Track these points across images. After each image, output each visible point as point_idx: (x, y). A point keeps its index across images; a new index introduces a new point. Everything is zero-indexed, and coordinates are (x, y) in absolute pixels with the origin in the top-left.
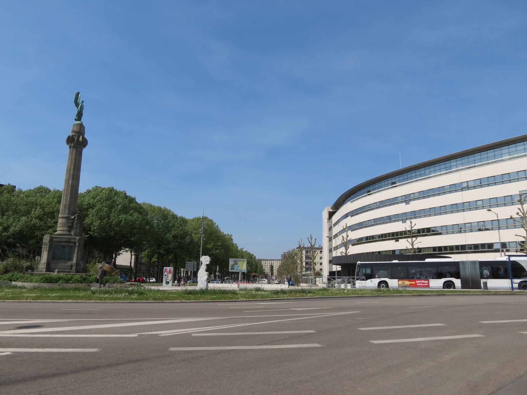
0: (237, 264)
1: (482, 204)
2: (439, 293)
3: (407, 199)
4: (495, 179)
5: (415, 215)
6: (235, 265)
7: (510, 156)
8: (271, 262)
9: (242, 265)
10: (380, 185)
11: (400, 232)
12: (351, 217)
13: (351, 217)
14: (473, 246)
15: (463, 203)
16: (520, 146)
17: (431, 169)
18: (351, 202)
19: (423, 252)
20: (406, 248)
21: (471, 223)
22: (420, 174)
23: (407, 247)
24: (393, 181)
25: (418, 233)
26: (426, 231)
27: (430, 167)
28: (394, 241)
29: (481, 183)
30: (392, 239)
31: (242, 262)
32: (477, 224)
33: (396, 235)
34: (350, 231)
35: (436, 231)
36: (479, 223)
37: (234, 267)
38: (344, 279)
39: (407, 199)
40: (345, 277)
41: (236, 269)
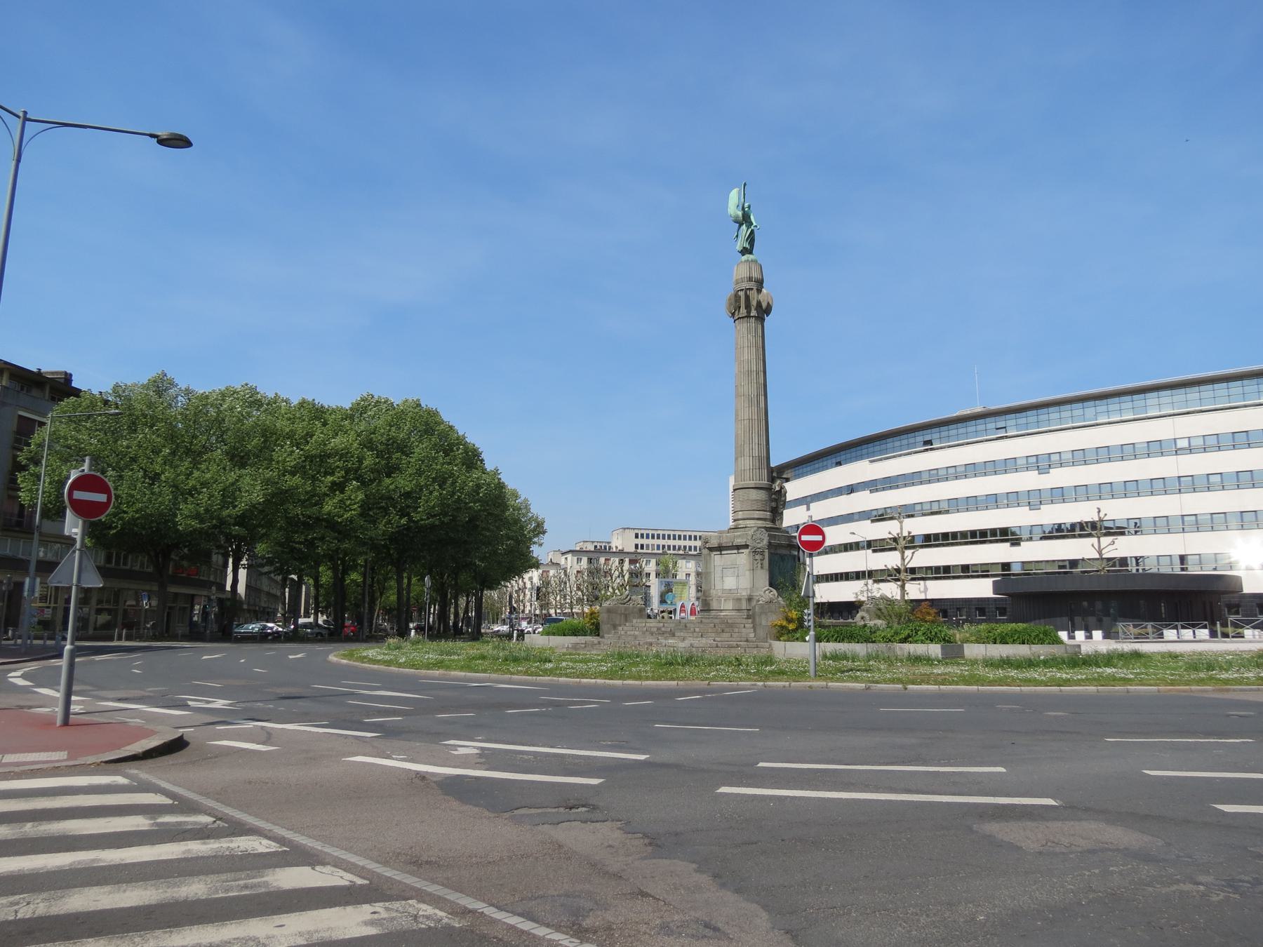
0: (672, 592)
1: (1220, 480)
2: (133, 609)
3: (1042, 464)
4: (1247, 436)
5: (909, 512)
6: (668, 593)
7: (1134, 415)
8: (1138, 570)
9: (681, 594)
10: (883, 447)
11: (991, 530)
12: (871, 493)
13: (871, 493)
14: (1067, 564)
15: (1179, 477)
16: (1250, 386)
17: (950, 431)
18: (871, 462)
19: (953, 573)
20: (884, 568)
21: (1196, 515)
22: (901, 446)
23: (886, 566)
24: (927, 438)
25: (1068, 531)
26: (959, 537)
27: (941, 430)
28: (1008, 544)
29: (1081, 457)
30: (1002, 541)
31: (681, 587)
32: (1209, 517)
33: (934, 538)
34: (869, 521)
35: (1065, 531)
36: (1214, 516)
37: (666, 597)
38: (1146, 627)
39: (1042, 464)
40: (1177, 623)
41: (669, 602)
